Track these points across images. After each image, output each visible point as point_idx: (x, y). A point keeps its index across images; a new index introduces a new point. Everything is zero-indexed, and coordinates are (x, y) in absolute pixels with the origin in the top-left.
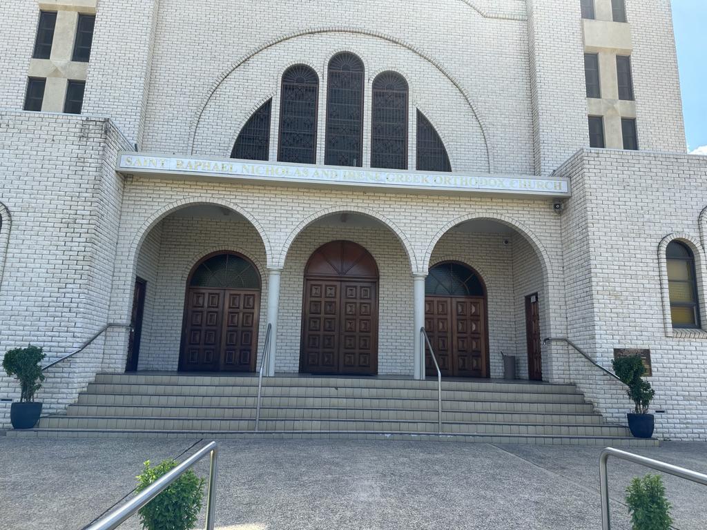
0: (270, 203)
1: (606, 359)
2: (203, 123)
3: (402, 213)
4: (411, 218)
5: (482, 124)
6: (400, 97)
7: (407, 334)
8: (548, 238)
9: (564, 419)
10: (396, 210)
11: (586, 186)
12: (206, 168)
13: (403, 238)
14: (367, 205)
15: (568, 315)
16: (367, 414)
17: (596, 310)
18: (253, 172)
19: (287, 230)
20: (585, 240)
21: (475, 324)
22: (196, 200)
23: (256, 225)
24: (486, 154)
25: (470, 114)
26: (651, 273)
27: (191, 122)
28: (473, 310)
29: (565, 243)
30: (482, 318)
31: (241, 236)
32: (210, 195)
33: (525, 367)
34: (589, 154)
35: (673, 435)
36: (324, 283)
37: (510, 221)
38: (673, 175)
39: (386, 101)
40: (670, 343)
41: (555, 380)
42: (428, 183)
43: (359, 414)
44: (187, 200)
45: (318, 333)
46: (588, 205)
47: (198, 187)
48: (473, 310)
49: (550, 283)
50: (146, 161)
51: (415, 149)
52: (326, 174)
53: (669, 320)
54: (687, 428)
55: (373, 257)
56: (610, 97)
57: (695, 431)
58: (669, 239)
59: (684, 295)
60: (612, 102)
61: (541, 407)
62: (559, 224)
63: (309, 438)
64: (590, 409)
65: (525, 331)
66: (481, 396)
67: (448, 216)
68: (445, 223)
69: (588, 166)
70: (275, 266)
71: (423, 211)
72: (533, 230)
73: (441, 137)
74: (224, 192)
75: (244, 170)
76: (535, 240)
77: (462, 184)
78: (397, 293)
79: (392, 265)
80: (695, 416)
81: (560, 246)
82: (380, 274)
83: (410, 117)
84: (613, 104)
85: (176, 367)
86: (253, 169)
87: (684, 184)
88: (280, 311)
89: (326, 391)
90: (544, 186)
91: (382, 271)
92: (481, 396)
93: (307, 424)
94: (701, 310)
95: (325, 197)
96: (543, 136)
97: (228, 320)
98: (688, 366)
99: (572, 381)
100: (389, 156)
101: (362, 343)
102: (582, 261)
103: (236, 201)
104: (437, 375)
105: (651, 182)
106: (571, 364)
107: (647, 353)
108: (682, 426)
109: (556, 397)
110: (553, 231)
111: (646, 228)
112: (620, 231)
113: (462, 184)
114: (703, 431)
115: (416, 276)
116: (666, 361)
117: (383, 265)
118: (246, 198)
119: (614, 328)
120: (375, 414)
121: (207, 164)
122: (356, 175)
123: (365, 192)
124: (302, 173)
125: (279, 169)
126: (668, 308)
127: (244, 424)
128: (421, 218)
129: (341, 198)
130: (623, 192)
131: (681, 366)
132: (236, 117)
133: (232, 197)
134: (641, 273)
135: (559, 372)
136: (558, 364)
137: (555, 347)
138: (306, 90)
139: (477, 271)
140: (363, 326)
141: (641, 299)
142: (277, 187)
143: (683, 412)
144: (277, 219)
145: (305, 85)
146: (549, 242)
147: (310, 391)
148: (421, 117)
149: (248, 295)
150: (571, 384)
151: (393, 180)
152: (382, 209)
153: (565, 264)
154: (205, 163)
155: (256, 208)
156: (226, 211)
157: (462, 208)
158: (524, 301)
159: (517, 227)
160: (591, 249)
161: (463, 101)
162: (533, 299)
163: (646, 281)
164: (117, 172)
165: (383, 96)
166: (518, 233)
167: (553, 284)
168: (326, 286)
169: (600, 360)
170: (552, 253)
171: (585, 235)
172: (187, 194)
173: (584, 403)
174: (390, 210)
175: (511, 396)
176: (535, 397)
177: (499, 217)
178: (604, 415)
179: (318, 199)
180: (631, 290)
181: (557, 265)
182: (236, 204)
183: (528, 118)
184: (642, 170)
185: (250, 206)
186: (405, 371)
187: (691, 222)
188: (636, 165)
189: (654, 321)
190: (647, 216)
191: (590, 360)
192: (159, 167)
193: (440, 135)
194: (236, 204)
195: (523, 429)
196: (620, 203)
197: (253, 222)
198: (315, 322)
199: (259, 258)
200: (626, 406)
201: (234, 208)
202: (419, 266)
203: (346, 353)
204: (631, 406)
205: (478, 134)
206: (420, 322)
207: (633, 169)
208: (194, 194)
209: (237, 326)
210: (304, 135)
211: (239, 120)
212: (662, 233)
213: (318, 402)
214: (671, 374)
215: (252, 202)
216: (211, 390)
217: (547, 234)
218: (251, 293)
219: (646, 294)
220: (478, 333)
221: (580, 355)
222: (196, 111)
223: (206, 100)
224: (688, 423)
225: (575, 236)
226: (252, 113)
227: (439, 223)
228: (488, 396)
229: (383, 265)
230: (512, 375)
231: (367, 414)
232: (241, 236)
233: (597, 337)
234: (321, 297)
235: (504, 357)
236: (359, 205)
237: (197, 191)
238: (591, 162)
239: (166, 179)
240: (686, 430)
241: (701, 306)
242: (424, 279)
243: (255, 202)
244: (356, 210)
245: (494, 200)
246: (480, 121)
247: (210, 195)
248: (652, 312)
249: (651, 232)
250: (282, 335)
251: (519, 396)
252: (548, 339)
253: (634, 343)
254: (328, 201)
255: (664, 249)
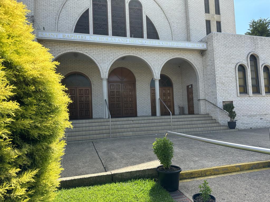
0: (100, 52)
1: (221, 105)
2: (61, 18)
3: (150, 56)
4: (153, 58)
5: (169, 22)
6: (96, 5)
7: (147, 102)
8: (199, 65)
9: (208, 125)
10: (148, 55)
11: (214, 46)
12: (75, 38)
13: (151, 66)
14: (137, 53)
15: (206, 91)
16: (146, 128)
17: (217, 89)
18: (102, 40)
19: (108, 63)
20: (213, 65)
21: (165, 97)
22: (70, 51)
23: (95, 61)
24: (171, 33)
25: (165, 18)
26: (233, 76)
27: (56, 18)
28: (168, 92)
29: (205, 66)
30: (171, 94)
31: (81, 66)
32: (76, 49)
33: (187, 110)
34: (214, 34)
35: (239, 127)
36: (115, 84)
37: (186, 59)
38: (240, 42)
39: (99, 7)
40: (239, 99)
41: (202, 113)
42: (160, 44)
43: (143, 128)
44: (66, 51)
45: (114, 103)
46: (214, 53)
47: (70, 46)
48: (168, 92)
49: (199, 81)
50: (49, 34)
51: (146, 31)
52: (122, 40)
53: (239, 91)
54: (243, 125)
55: (133, 74)
56: (213, 13)
57: (245, 126)
58: (239, 64)
59: (242, 84)
60: (213, 15)
61: (200, 122)
62: (202, 60)
63: (130, 138)
64: (215, 121)
65: (187, 98)
66: (181, 120)
67: (166, 57)
68: (165, 60)
69: (214, 39)
70: (104, 77)
71: (157, 55)
72: (194, 62)
73: (155, 26)
74: (81, 48)
75: (91, 39)
76: (195, 65)
77: (172, 45)
78: (143, 87)
79: (140, 76)
80: (245, 121)
81: (203, 67)
82: (136, 80)
83: (144, 18)
84: (214, 16)
85: (151, 114)
86: (94, 38)
87: (243, 45)
88: (102, 95)
89: (129, 122)
90: (199, 46)
91: (137, 79)
92: (181, 120)
93: (128, 133)
94: (247, 88)
95: (121, 50)
96: (191, 27)
97: (79, 99)
98: (244, 106)
99: (207, 113)
100: (137, 33)
101: (131, 106)
102: (212, 72)
103: (87, 51)
104: (170, 115)
105: (233, 44)
106: (207, 107)
107: (232, 102)
108: (242, 124)
109: (204, 118)
110: (200, 62)
111: (232, 60)
112: (224, 62)
113: (172, 45)
114: (247, 125)
115: (156, 80)
116: (237, 104)
117: (137, 76)
118: (90, 50)
119: (223, 94)
120: (149, 128)
121: (75, 36)
122: (134, 41)
123: (136, 48)
124: (113, 40)
125: (105, 38)
126: (238, 87)
127: (105, 135)
128: (157, 58)
129: (127, 50)
130: (225, 48)
131: (242, 106)
132: (75, 16)
133: (84, 50)
134: (230, 76)
135: (203, 110)
136: (203, 108)
137: (202, 102)
138: (138, 10)
139: (169, 78)
140: (131, 100)
141: (230, 84)
142: (102, 45)
143: (242, 120)
144: (103, 59)
145: (102, 3)
146: (199, 66)
147: (124, 123)
148: (147, 18)
149: (86, 89)
150: (207, 114)
151: (148, 43)
152: (142, 55)
153: (204, 74)
154: (74, 36)
155: (95, 54)
156: (76, 55)
157: (171, 54)
158: (186, 88)
159: (189, 61)
160: (216, 68)
161: (162, 13)
162: (190, 87)
163: (232, 79)
164: (37, 39)
165: (97, 5)
166: (186, 61)
167: (201, 81)
168: (116, 85)
169: (218, 105)
170: (200, 70)
171: (213, 63)
172: (66, 49)
173: (212, 120)
174: (145, 55)
175: (190, 119)
176: (197, 119)
177: (183, 57)
178: (220, 123)
179: (118, 51)
180: (228, 82)
181: (202, 74)
182: (86, 53)
183: (185, 20)
184: (230, 40)
185: (92, 53)
186: (147, 114)
187: (245, 59)
188: (229, 39)
189: (234, 92)
190: (232, 56)
191: (215, 105)
192: (55, 37)
193: (155, 25)
194: (86, 53)
195: (197, 129)
196: (224, 52)
197: (94, 60)
198: (113, 99)
199: (90, 75)
200: (226, 119)
201: (86, 54)
202: (157, 76)
203: (125, 110)
204: (229, 119)
205: (168, 26)
206: (106, 97)
207: (228, 40)
208: (69, 49)
209: (83, 102)
210: (103, 24)
211: (76, 18)
212: (236, 62)
213: (128, 126)
214: (239, 109)
215: (93, 52)
216: (87, 125)
217: (198, 63)
218: (88, 89)
219: (232, 83)
220: (170, 100)
221: (209, 103)
222: (57, 13)
223: (61, 8)
224: (244, 123)
225: (209, 64)
226: (81, 15)
227: (163, 60)
228: (183, 120)
229: (137, 76)
230: (182, 112)
231: (146, 128)
232: (81, 66)
233: (218, 98)
234: (114, 89)
235: (179, 107)
236: (134, 53)
237: (70, 47)
238: (215, 37)
239: (57, 42)
240: (243, 126)
241: (247, 86)
242: (158, 81)
243: (94, 52)
244: (133, 55)
245: (181, 51)
246: (169, 21)
247: (76, 49)
248: (234, 89)
249: (233, 62)
250: (101, 104)
251: (192, 119)
252: (199, 100)
253: (229, 99)
254: (122, 51)
255: (237, 67)
